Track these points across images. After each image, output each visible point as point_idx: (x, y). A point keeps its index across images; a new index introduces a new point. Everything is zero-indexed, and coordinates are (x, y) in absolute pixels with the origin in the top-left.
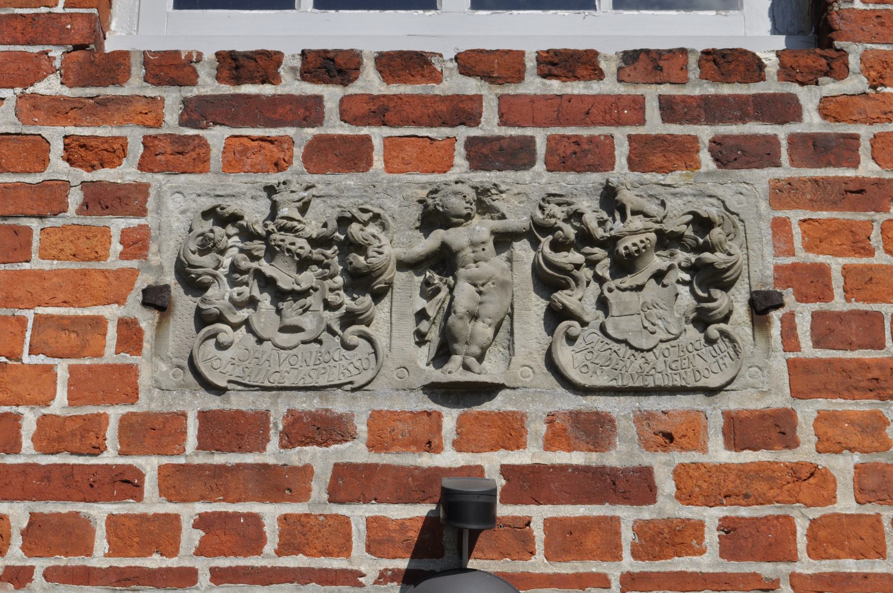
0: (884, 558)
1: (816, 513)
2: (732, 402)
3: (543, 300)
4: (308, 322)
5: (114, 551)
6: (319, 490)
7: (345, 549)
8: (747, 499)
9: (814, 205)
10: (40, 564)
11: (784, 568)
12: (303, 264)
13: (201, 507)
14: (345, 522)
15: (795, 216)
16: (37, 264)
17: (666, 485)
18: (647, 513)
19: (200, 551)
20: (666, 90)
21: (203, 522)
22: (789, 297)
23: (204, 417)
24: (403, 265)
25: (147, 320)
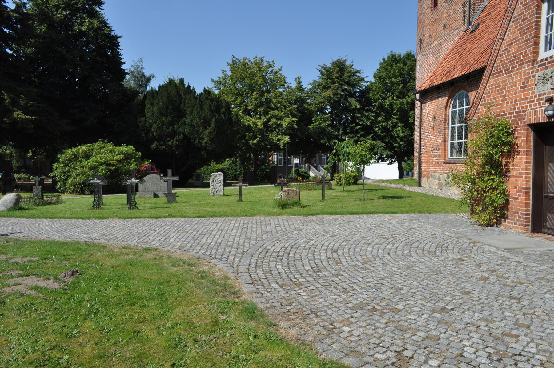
0: (530, 125)
12: (543, 80)
21: (538, 103)
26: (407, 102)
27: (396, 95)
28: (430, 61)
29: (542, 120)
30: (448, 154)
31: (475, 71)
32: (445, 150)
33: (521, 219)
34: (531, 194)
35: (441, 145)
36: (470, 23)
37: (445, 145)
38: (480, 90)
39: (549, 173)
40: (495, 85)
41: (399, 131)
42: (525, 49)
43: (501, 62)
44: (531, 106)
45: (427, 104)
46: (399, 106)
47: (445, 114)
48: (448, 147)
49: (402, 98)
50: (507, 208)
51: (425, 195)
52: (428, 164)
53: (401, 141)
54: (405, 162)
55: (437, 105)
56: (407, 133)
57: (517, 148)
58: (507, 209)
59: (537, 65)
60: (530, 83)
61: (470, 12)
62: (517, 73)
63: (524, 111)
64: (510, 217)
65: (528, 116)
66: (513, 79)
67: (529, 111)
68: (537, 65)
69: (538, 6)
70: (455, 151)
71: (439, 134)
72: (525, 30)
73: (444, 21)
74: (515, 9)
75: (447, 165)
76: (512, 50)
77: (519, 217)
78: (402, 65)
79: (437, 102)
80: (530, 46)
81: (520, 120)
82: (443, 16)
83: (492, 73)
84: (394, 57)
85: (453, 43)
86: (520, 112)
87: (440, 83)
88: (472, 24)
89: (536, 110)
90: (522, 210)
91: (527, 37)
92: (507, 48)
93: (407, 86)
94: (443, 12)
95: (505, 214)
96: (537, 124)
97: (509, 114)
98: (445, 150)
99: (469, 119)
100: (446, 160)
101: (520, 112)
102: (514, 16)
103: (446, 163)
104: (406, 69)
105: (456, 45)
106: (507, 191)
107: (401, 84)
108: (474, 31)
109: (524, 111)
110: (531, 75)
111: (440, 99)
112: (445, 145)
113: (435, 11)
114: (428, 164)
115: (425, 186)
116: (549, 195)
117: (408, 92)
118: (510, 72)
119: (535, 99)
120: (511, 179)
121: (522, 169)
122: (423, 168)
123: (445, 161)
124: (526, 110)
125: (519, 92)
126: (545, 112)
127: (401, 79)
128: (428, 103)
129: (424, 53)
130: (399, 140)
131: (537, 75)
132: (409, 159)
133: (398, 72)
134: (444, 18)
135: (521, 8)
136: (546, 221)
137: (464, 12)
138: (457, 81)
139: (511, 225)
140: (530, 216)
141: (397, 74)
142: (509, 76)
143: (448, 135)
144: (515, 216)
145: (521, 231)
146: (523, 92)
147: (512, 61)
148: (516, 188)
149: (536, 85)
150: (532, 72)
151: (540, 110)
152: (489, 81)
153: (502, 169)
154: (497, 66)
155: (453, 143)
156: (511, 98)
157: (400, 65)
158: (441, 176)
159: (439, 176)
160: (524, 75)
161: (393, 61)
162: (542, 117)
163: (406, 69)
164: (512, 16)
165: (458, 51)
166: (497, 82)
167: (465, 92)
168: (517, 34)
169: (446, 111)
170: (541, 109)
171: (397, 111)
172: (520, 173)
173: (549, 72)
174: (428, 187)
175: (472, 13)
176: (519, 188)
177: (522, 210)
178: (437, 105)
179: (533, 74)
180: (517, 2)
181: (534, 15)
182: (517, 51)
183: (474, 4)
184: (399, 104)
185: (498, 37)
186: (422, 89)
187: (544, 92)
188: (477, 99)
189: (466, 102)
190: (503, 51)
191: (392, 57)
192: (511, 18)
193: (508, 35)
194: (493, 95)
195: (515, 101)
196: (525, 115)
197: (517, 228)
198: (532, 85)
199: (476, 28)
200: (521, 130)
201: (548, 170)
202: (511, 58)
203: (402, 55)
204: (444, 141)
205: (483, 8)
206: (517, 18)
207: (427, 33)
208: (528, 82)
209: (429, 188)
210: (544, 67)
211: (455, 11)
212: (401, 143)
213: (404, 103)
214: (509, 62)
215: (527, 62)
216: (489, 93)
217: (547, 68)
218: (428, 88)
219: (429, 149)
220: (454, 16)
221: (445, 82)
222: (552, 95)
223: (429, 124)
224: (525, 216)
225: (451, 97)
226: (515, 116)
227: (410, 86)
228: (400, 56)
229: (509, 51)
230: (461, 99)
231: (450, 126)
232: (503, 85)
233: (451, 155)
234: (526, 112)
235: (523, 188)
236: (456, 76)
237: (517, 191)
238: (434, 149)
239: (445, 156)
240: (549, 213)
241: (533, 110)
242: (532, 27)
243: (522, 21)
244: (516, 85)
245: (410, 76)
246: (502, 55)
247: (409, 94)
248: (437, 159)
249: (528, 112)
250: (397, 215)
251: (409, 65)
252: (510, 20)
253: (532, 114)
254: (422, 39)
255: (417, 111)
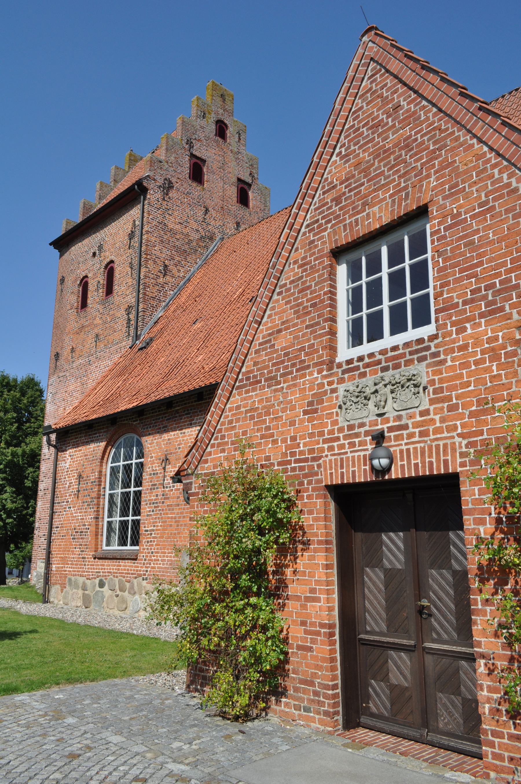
0: (328, 487)
1: (433, 427)
2: (421, 408)
3: (143, 442)
4: (359, 407)
5: (338, 450)
6: (363, 435)
7: (367, 445)
8: (423, 426)
9: (433, 367)
10: (329, 454)
11: (428, 438)
12: (357, 397)
13: (348, 441)
14: (366, 440)
15: (430, 370)
16: (325, 404)
17: (410, 426)
18: (408, 431)
19: (349, 448)
20: (410, 349)
21: (349, 443)
22: (429, 387)
23: (347, 426)
24: (372, 394)
25: (339, 411)
26: (24, 452)
27: (6, 439)
28: (71, 388)
29: (360, 477)
30: (102, 541)
31: (156, 401)
32: (97, 535)
33: (321, 699)
34: (337, 637)
35: (90, 525)
36: (137, 337)
37: (97, 525)
38: (212, 416)
39: (366, 590)
40: (244, 407)
41: (6, 500)
42: (309, 340)
43: (256, 364)
44: (331, 448)
45: (68, 452)
46: (10, 458)
47: (100, 472)
48: (103, 528)
49: (16, 446)
50: (284, 670)
51: (62, 624)
52: (64, 561)
53: (9, 517)
54: (11, 552)
55: (86, 456)
56: (20, 502)
57: (303, 536)
58: (285, 674)
59: (340, 370)
60: (325, 404)
61: (137, 322)
62: (295, 385)
63: (314, 459)
64: (291, 692)
65: (325, 469)
66: (285, 396)
67: (327, 459)
68: (340, 370)
69: (331, 266)
70: (116, 538)
71: (88, 505)
72: (307, 306)
73: (96, 331)
74: (282, 271)
75: (100, 562)
76: (281, 343)
77: (316, 694)
78: (18, 395)
79: (86, 449)
80: (321, 335)
81: (305, 476)
82: (95, 322)
83: (237, 384)
84: (6, 380)
85: (110, 363)
86: (306, 460)
87: (94, 417)
88: (139, 339)
89: (344, 456)
90: (323, 677)
91: (313, 318)
92: (270, 340)
93: (24, 428)
94: (96, 316)
95: (276, 686)
96: (348, 485)
97: (279, 464)
98: (97, 535)
99: (185, 473)
100: (99, 553)
101: (306, 460)
102: (281, 283)
103: (99, 559)
104: (25, 402)
105: (116, 364)
106: (282, 631)
107: (15, 422)
108: (145, 347)
109: (314, 459)
110: (326, 387)
111: (92, 446)
112: (97, 525)
113: (82, 314)
114: (64, 561)
115: (56, 602)
116: (372, 638)
117: (26, 437)
118: (279, 383)
119: (341, 435)
120: (290, 603)
121: (318, 582)
122: (54, 566)
123: (98, 554)
124: (322, 457)
125: (302, 421)
126: (371, 459)
127: (15, 415)
128: (70, 451)
129: (61, 374)
130: (4, 516)
131: (341, 388)
132: (17, 548)
133: (11, 404)
134: (96, 326)
135: (296, 270)
136: (368, 697)
137: (129, 320)
138: (122, 417)
139: (297, 712)
140: (339, 691)
141: (9, 406)
142: (276, 391)
143: (103, 508)
144: (305, 691)
145: (322, 728)
146: (310, 420)
147: (283, 362)
148: (303, 623)
149: (340, 407)
150: (328, 382)
151: (353, 457)
152: (231, 399)
153: (269, 581)
154: (248, 372)
155: (112, 522)
156: (283, 433)
157: (15, 393)
158: (88, 582)
159: (84, 583)
160: (311, 389)
161: (5, 386)
162: (359, 471)
163: (25, 402)
164: (277, 284)
165: (120, 375)
166: (250, 402)
167: (136, 437)
168: (290, 314)
169: (101, 466)
170: (356, 454)
171: (6, 466)
172: (313, 591)
173: (371, 383)
174: (61, 602)
175: (140, 324)
176: (313, 624)
177: (323, 677)
178: (86, 456)
179: (333, 387)
180: (287, 261)
181: (325, 281)
182: (293, 345)
183: (144, 311)
184: (9, 454)
185: (250, 318)
186: (60, 425)
187: (360, 421)
188: (205, 433)
189: (137, 452)
190: (260, 344)
191: (3, 380)
192: (275, 287)
193: (270, 316)
194: (240, 427)
195: (294, 439)
196: (319, 466)
197: (313, 720)
198: (331, 407)
199: (148, 344)
200: (309, 497)
201: (363, 583)
202: (279, 356)
203: (19, 380)
204: (97, 518)
205: (156, 319)
206: (288, 286)
207: (68, 343)
208: (321, 402)
209: (63, 605)
210: (357, 373)
211: (114, 318)
212: (8, 521)
213: (17, 454)
214: (274, 365)
215: (316, 365)
216: (231, 422)
217: (363, 375)
218: (73, 425)
219: (68, 533)
220: (112, 324)
221: (103, 417)
222: (380, 427)
223: (69, 487)
224: (330, 692)
225: (110, 443)
226: (294, 469)
227: (28, 428)
228: (15, 380)
229: (274, 345)
230: (129, 447)
231: (108, 492)
232: (264, 407)
233: (108, 544)
234: (321, 461)
235: (322, 626)
236: (123, 409)
237: (306, 632)
238: (77, 532)
239: (96, 545)
240: (374, 678)
241: (339, 457)
242: (322, 301)
243: (300, 292)
244: (293, 408)
245: (30, 413)
246: (257, 352)
247: (27, 441)
248: (82, 551)
249: (325, 462)
250: (19, 698)
251: (30, 394)
252: (274, 291)
253: (336, 465)
254: (60, 352)
255: (46, 467)
